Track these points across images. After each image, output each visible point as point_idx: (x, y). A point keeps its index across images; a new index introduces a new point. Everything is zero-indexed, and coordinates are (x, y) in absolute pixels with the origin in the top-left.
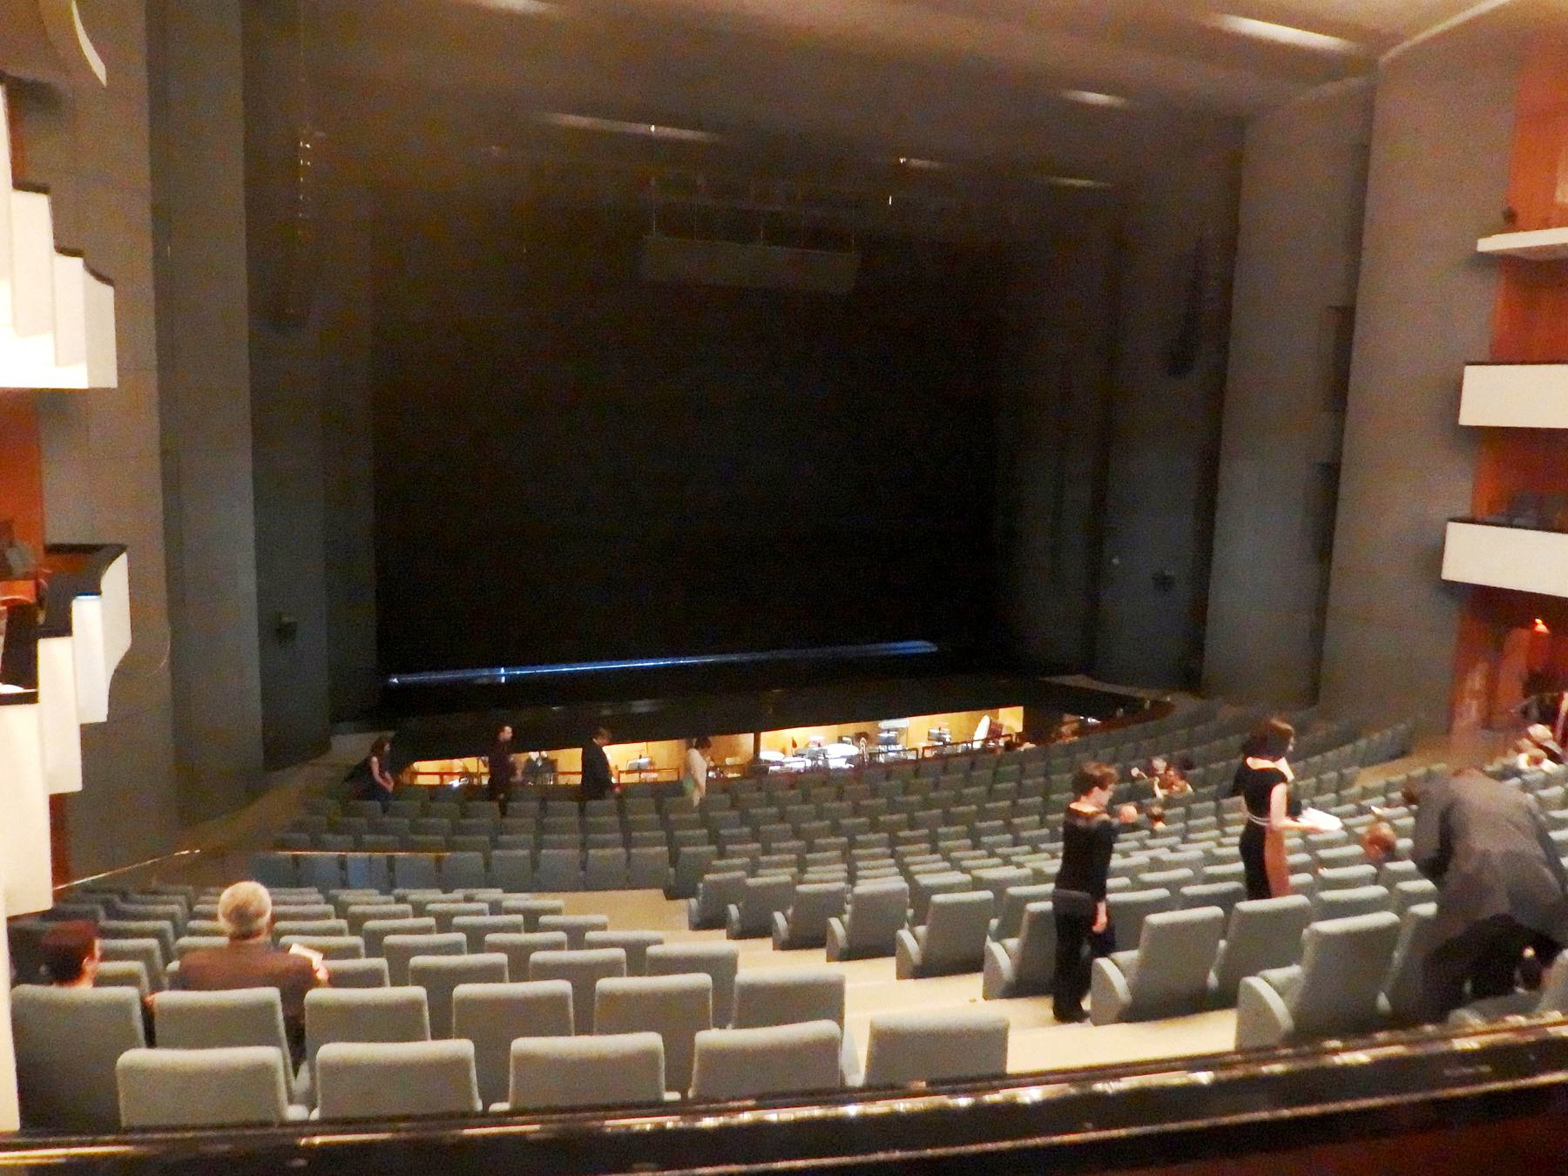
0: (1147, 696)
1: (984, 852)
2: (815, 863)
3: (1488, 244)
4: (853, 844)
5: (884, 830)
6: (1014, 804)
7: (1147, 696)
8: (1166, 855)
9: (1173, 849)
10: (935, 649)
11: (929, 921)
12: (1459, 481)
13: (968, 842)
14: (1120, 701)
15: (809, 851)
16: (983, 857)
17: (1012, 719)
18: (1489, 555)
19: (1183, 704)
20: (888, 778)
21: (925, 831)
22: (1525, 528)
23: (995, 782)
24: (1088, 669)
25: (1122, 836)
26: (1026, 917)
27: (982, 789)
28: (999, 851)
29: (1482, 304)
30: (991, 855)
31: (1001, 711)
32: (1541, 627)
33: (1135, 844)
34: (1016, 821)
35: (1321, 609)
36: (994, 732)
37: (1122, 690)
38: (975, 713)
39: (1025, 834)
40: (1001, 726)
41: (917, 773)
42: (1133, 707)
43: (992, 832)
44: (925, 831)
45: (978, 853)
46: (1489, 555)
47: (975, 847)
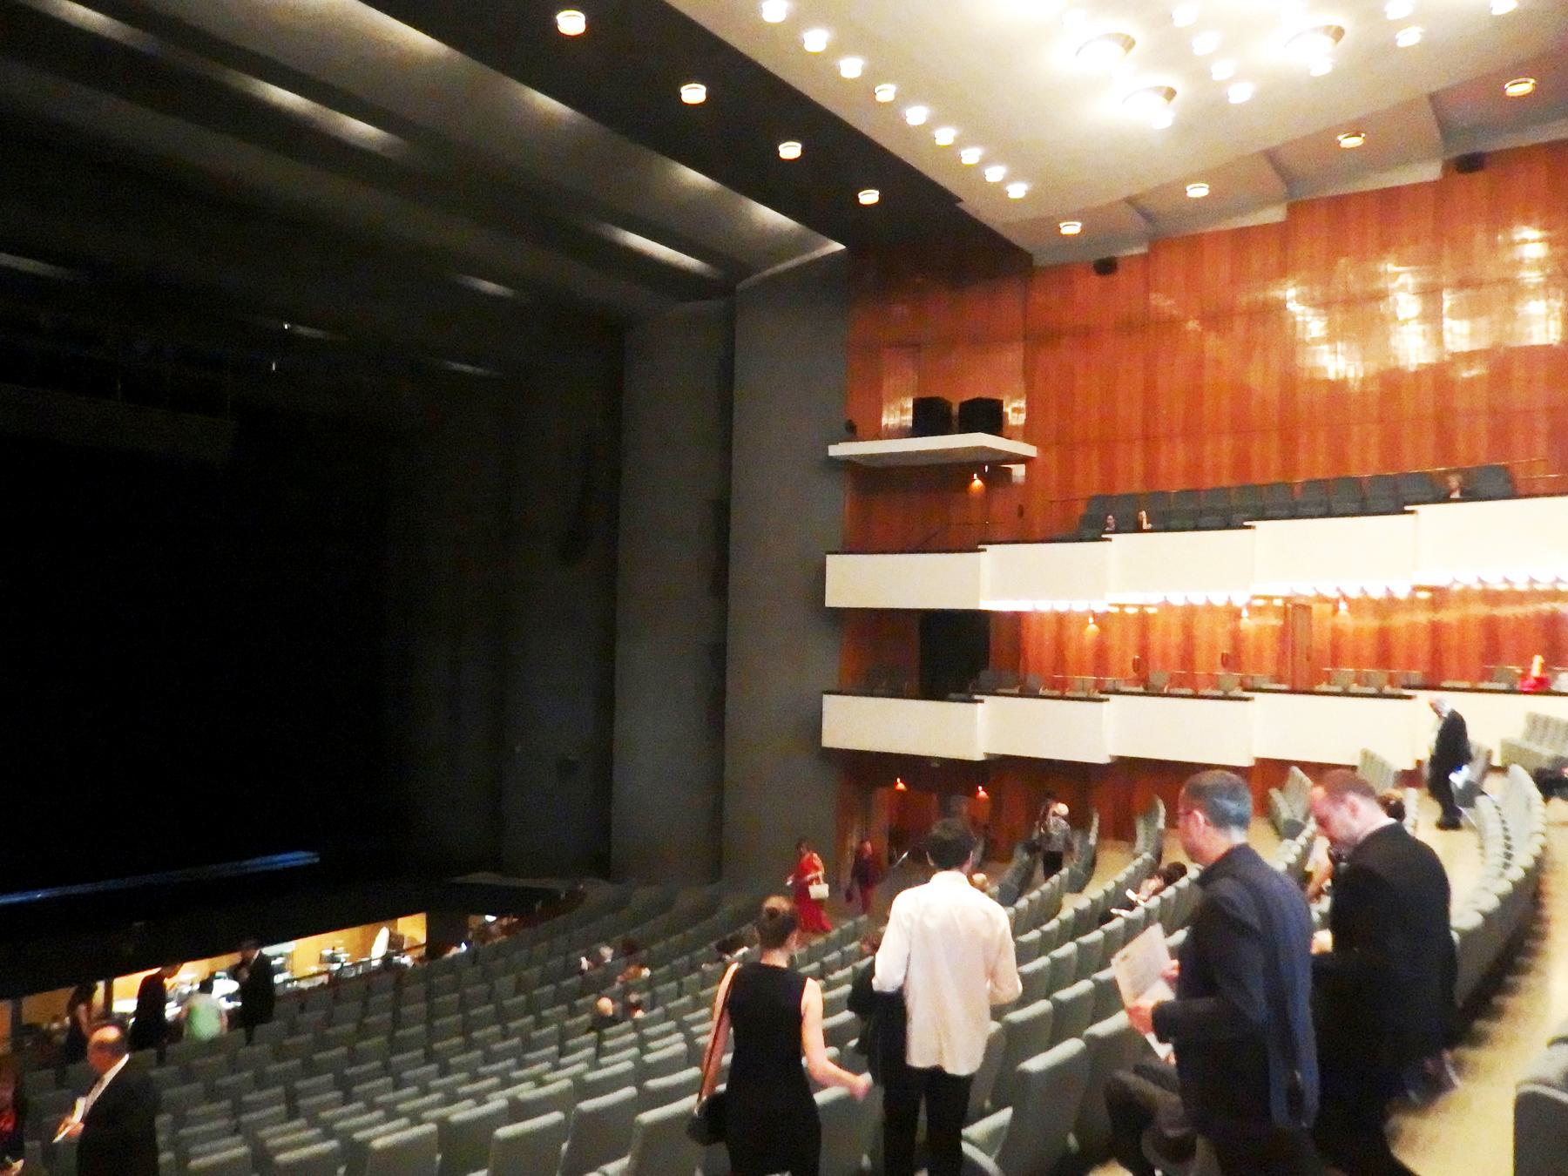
0: (559, 886)
1: (360, 1105)
2: (196, 1139)
3: (839, 450)
4: (238, 1109)
5: (276, 1084)
6: (391, 1038)
7: (559, 886)
8: (526, 1092)
9: (540, 1082)
10: (317, 860)
11: (491, 1164)
12: (825, 656)
13: (337, 1094)
14: (531, 895)
15: (393, 1053)
16: (361, 1113)
17: (413, 928)
18: (864, 723)
19: (597, 891)
20: (302, 1008)
21: (377, 1064)
22: (1312, 517)
23: (365, 1015)
24: (497, 865)
25: (197, 1149)
26: (491, 1164)
27: (350, 1027)
28: (381, 1099)
29: (836, 500)
30: (371, 1107)
31: (400, 921)
32: (901, 786)
33: (494, 1081)
34: (396, 1059)
35: (717, 782)
36: (396, 944)
37: (536, 884)
38: (367, 928)
39: (408, 1074)
40: (402, 937)
41: (337, 999)
42: (549, 897)
43: (416, 1064)
44: (279, 1090)
45: (297, 1123)
46: (864, 723)
47: (347, 1099)
